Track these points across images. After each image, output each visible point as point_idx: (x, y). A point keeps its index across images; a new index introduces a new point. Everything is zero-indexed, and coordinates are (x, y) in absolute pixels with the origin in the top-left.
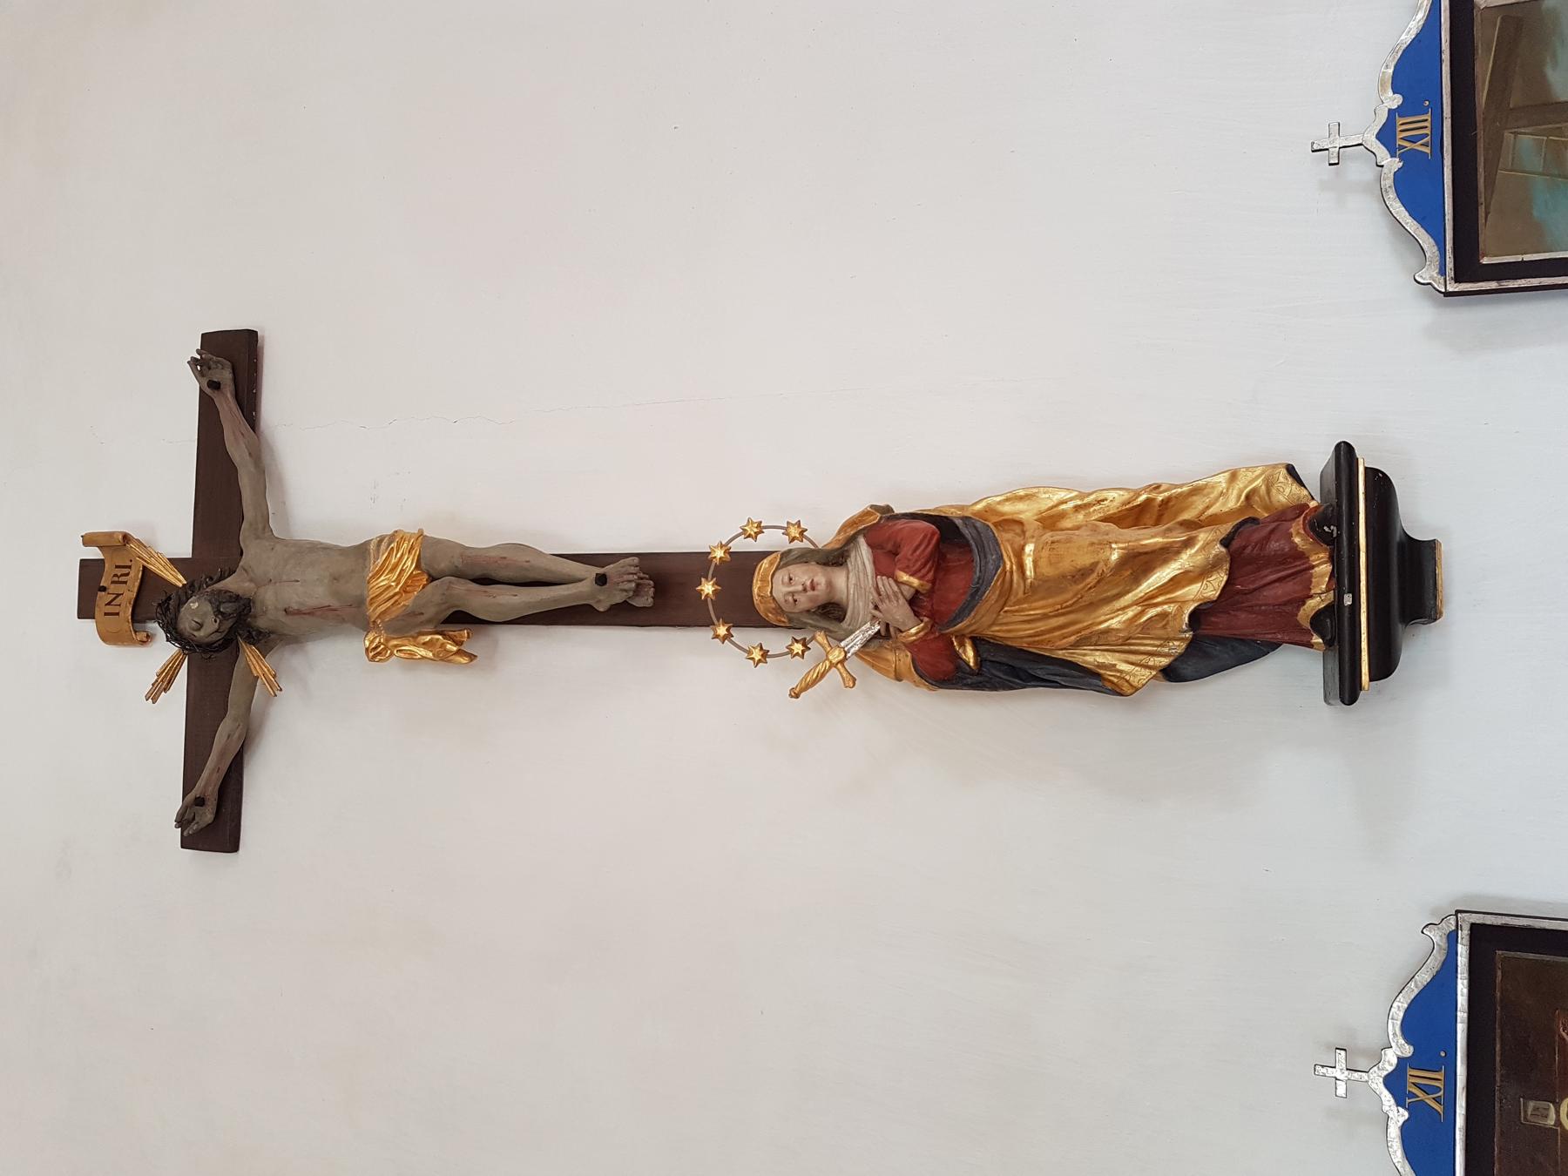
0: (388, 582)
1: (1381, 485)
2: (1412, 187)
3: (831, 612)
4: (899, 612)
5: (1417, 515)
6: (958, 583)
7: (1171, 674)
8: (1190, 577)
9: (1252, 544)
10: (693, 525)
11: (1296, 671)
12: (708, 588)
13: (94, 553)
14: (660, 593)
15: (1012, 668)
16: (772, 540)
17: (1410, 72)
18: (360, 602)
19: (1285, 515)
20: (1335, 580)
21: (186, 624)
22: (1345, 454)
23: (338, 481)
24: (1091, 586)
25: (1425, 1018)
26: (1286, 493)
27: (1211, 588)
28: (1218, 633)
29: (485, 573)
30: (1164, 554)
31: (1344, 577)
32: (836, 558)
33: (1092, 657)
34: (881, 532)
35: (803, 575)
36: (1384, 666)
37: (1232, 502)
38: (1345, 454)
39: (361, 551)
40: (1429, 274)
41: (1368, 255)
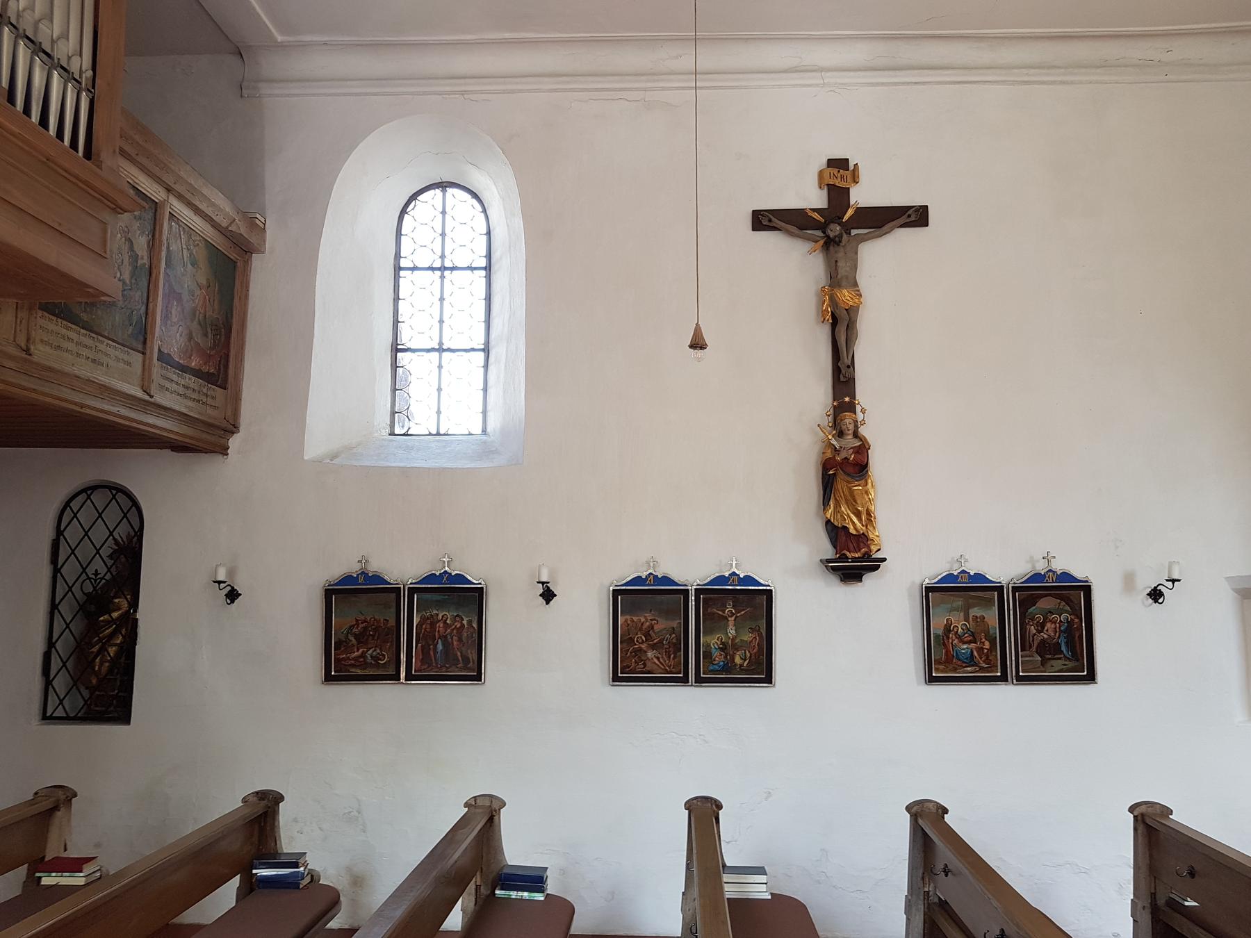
0: (845, 295)
1: (876, 568)
2: (949, 577)
3: (841, 434)
4: (844, 454)
5: (869, 578)
6: (850, 469)
7: (828, 522)
8: (855, 525)
9: (862, 540)
10: (863, 393)
11: (828, 552)
12: (847, 399)
13: (851, 166)
14: (843, 380)
15: (827, 486)
16: (860, 416)
17: (980, 577)
18: (840, 286)
19: (869, 547)
20: (852, 559)
21: (832, 226)
22: (884, 560)
23: (878, 259)
24: (852, 501)
25: (749, 580)
26: (874, 548)
27: (852, 531)
28: (105, 380)
29: (851, 328)
30: (860, 520)
31: (855, 560)
32: (856, 435)
33: (832, 503)
34: (863, 449)
35: (851, 427)
36: (834, 569)
37: (871, 536)
38: (884, 560)
39: (856, 285)
40: (927, 581)
41: (934, 568)
